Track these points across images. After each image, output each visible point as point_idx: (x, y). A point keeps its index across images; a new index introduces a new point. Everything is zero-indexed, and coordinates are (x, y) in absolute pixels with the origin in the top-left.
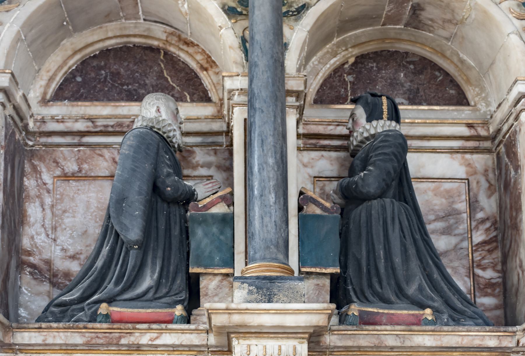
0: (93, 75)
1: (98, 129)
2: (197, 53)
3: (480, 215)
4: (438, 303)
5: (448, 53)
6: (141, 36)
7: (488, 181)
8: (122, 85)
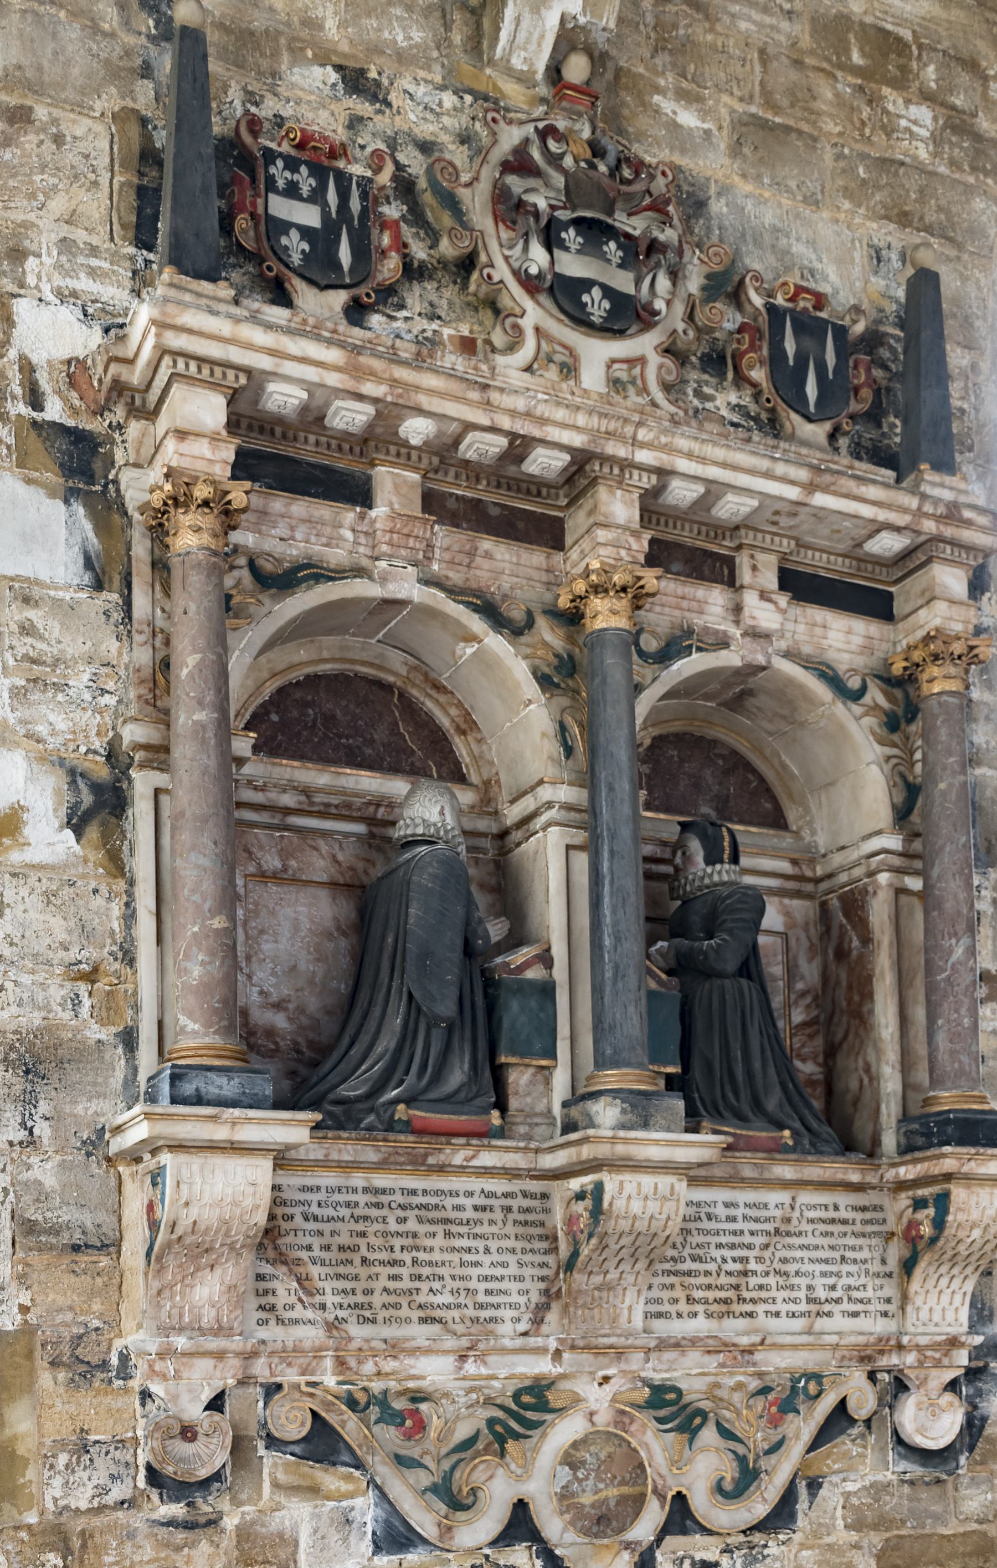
0: (295, 714)
1: (315, 809)
2: (451, 704)
3: (800, 986)
4: (797, 1125)
5: (768, 752)
6: (371, 665)
7: (808, 938)
8: (340, 737)
